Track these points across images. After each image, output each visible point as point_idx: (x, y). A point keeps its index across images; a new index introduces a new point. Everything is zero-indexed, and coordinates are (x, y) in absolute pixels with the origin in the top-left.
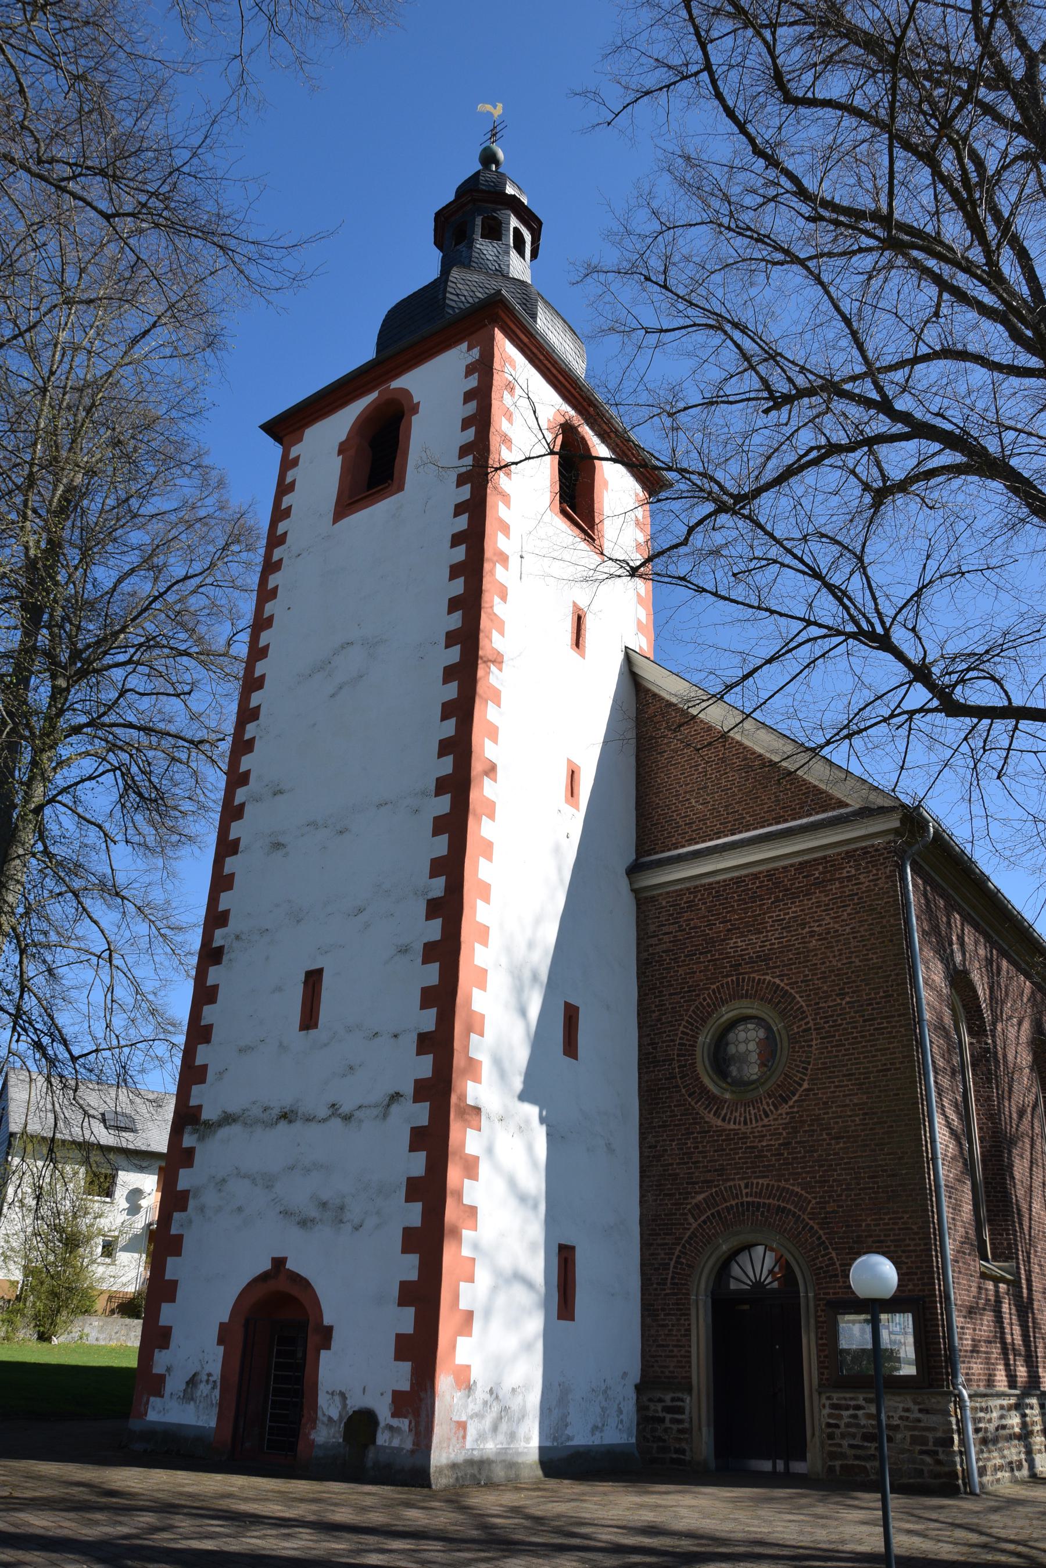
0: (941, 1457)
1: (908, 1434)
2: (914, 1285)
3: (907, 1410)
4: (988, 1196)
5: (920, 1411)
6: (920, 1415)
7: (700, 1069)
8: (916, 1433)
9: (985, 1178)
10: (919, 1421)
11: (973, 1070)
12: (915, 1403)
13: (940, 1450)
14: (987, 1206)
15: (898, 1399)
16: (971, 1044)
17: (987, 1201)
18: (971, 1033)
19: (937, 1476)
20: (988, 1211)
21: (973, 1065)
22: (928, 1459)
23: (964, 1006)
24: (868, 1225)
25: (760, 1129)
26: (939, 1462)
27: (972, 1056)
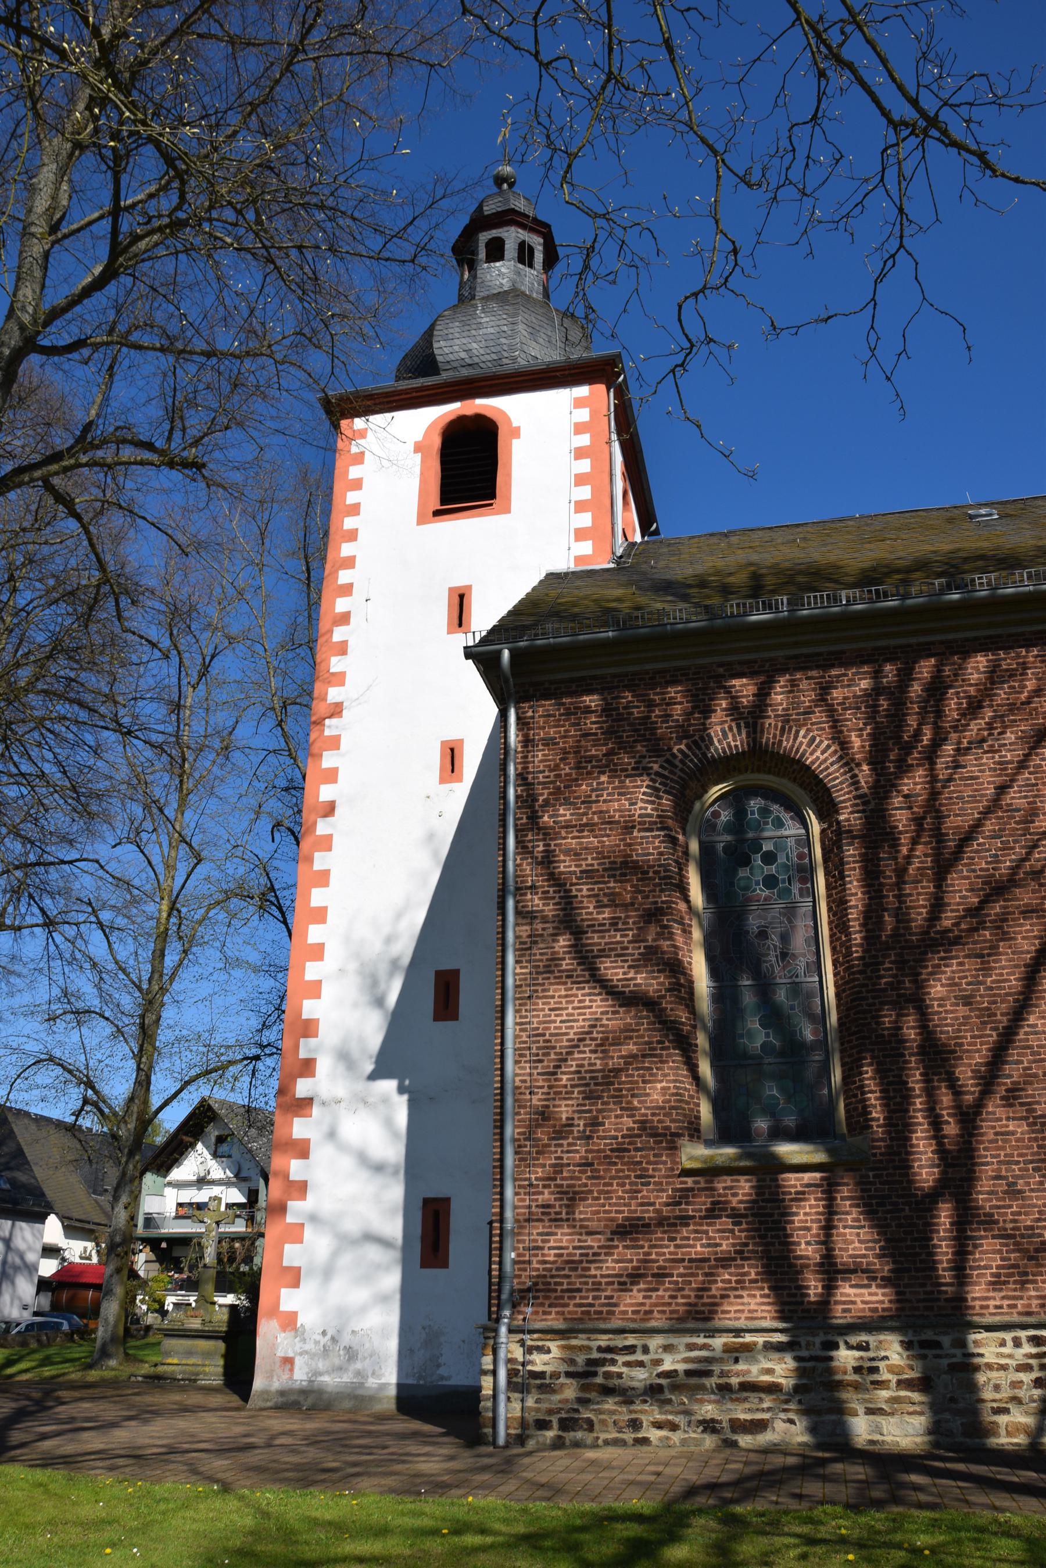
9: (839, 1019)
11: (826, 868)
14: (842, 1059)
18: (821, 818)
20: (843, 1065)
23: (801, 785)
25: (580, 992)
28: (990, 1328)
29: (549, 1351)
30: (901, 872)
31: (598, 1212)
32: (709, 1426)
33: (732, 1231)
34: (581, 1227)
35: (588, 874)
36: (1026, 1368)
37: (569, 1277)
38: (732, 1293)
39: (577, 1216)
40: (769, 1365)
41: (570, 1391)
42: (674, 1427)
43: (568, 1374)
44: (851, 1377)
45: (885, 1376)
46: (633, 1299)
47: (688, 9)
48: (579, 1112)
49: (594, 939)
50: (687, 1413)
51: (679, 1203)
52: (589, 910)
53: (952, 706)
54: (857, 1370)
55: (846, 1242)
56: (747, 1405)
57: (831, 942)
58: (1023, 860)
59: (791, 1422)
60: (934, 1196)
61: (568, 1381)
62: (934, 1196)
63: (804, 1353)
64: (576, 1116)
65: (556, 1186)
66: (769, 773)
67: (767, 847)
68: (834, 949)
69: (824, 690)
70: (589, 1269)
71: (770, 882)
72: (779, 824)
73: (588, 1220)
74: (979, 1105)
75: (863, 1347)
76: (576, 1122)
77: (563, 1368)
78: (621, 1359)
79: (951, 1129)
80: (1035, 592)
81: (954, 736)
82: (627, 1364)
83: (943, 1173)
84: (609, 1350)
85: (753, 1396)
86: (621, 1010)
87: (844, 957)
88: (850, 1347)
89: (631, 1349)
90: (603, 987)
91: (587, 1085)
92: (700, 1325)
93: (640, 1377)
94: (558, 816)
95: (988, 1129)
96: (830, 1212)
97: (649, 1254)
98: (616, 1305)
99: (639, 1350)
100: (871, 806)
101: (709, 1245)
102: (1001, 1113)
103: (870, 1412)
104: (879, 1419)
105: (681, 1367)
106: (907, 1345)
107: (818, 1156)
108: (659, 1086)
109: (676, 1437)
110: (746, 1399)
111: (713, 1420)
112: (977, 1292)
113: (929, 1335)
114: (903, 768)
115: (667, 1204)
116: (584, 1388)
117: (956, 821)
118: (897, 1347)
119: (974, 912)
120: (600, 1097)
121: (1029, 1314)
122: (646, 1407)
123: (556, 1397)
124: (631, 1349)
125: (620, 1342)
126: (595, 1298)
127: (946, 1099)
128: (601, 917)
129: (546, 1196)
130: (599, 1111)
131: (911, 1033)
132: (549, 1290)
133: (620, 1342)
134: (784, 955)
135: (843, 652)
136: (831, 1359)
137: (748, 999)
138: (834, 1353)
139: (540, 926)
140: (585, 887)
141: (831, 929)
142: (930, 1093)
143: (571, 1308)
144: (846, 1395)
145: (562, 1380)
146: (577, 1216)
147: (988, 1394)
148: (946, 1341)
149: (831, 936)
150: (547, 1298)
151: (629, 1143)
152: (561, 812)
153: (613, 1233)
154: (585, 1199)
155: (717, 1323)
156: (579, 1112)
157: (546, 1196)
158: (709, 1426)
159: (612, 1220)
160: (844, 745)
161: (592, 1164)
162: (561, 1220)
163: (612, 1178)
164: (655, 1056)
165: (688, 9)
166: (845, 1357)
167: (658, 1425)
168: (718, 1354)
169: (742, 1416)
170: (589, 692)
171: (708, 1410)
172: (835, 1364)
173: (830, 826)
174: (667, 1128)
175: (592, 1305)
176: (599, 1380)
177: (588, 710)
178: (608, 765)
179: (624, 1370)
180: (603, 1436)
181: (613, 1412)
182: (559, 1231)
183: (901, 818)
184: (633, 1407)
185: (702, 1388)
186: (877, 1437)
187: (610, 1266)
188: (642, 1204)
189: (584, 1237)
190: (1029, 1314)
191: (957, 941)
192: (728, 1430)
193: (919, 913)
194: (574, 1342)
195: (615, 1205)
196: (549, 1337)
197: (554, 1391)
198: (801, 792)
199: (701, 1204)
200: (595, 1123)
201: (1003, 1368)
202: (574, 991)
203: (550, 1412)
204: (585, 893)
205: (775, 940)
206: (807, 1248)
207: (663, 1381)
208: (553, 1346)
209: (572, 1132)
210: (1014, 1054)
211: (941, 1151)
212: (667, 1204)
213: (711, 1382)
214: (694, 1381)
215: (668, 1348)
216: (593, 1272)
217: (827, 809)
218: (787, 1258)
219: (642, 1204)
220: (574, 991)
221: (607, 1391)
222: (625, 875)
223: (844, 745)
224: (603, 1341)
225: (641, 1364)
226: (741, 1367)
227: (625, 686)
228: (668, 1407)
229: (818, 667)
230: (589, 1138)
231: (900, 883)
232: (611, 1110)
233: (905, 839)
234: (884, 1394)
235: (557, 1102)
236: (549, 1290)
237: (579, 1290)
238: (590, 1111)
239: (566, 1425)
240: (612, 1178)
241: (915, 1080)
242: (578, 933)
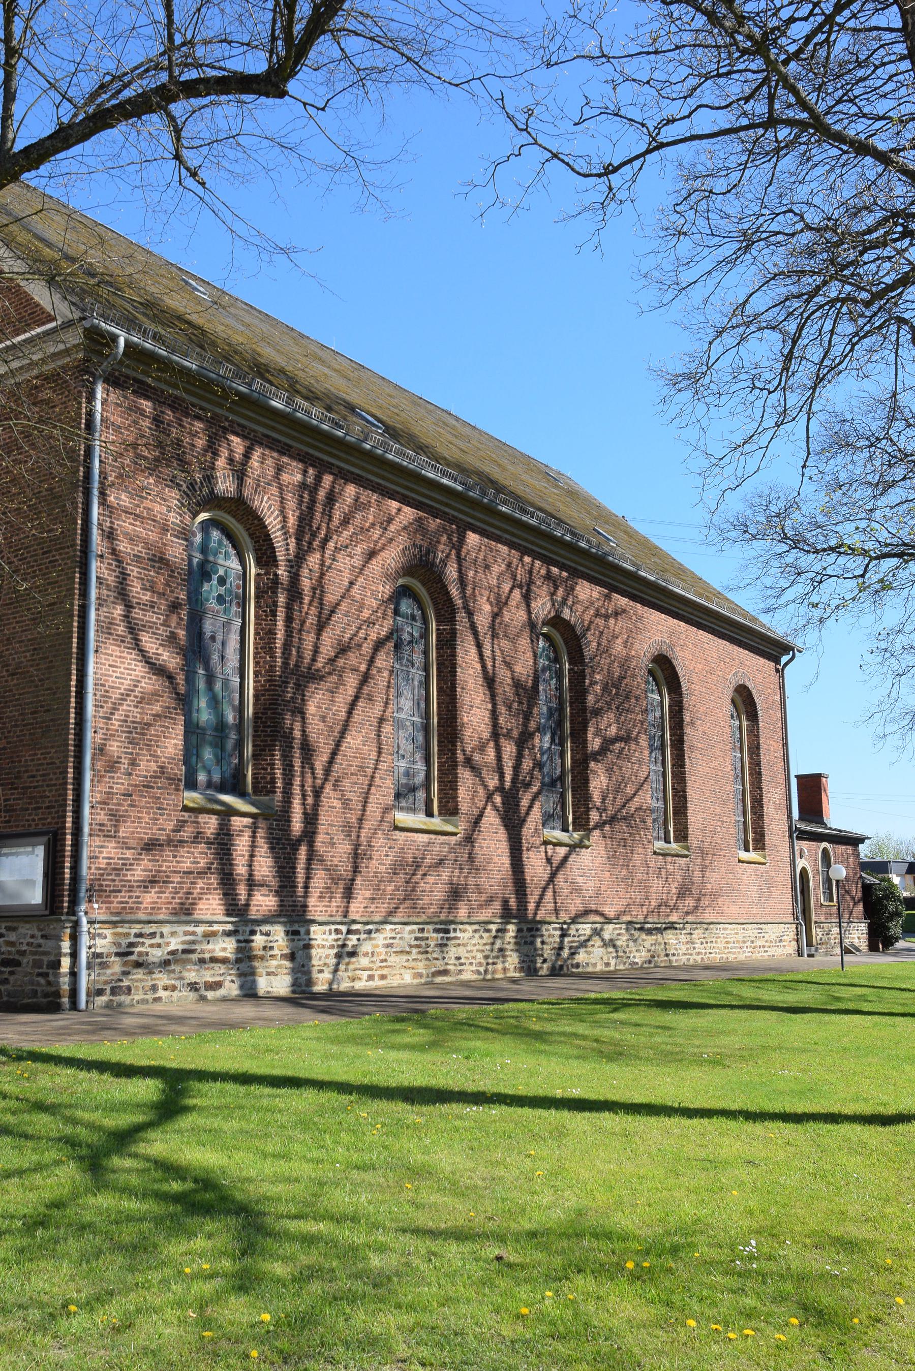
0: (51, 978)
1: (31, 958)
2: (53, 818)
3: (32, 936)
4: (255, 731)
5: (42, 936)
6: (41, 941)
7: (419, 585)
8: (37, 957)
9: (255, 713)
10: (40, 946)
11: (257, 603)
12: (40, 930)
13: (51, 971)
14: (254, 741)
15: (28, 926)
16: (258, 575)
17: (254, 736)
18: (259, 563)
19: (46, 995)
20: (254, 746)
21: (257, 597)
22: (42, 981)
23: (250, 535)
24: (26, 761)
25: (129, 656)
26: (49, 983)
27: (257, 588)
28: (321, 924)
29: (105, 937)
30: (303, 622)
31: (133, 833)
32: (193, 987)
33: (206, 854)
34: (124, 843)
35: (137, 558)
36: (332, 947)
37: (114, 880)
38: (204, 897)
39: (121, 834)
40: (224, 945)
41: (116, 967)
42: (174, 988)
43: (117, 954)
44: (261, 953)
45: (276, 952)
46: (149, 898)
47: (522, 130)
48: (126, 753)
49: (137, 613)
50: (181, 978)
51: (179, 831)
52: (136, 589)
53: (337, 515)
54: (265, 948)
55: (261, 866)
56: (212, 972)
57: (255, 658)
58: (355, 635)
59: (233, 981)
60: (299, 841)
61: (117, 959)
62: (299, 841)
63: (241, 938)
64: (123, 756)
65: (109, 810)
66: (234, 517)
67: (221, 572)
68: (257, 663)
69: (279, 469)
70: (126, 875)
71: (220, 599)
72: (227, 556)
73: (128, 838)
74: (322, 787)
75: (267, 934)
76: (123, 760)
77: (114, 950)
78: (148, 942)
79: (310, 800)
80: (317, 426)
81: (335, 537)
82: (151, 946)
83: (305, 827)
84: (140, 935)
85: (216, 966)
86: (154, 677)
87: (267, 671)
88: (262, 934)
89: (153, 935)
90: (144, 656)
91: (130, 732)
92: (184, 918)
93: (157, 955)
94: (120, 499)
95: (324, 801)
96: (253, 846)
97: (161, 866)
98: (141, 903)
99: (158, 935)
100: (294, 570)
101: (194, 863)
102: (332, 794)
103: (268, 974)
104: (272, 978)
105: (180, 947)
106: (287, 933)
107: (253, 810)
108: (173, 741)
109: (176, 994)
110: (213, 968)
111: (196, 983)
112: (312, 901)
113: (296, 927)
114: (310, 549)
115: (174, 831)
116: (125, 964)
117: (330, 598)
118: (282, 934)
119: (332, 661)
120: (138, 744)
121: (331, 916)
122: (161, 975)
123: (109, 971)
124: (153, 935)
125: (148, 929)
126: (130, 897)
127: (309, 781)
128: (145, 598)
129: (102, 817)
130: (137, 754)
131: (297, 734)
132: (102, 891)
133: (148, 929)
134: (223, 657)
135: (291, 447)
136: (252, 941)
137: (202, 685)
138: (253, 938)
139: (105, 592)
140: (136, 569)
141: (256, 648)
142: (303, 774)
143: (115, 905)
144: (256, 964)
145: (113, 959)
146: (121, 834)
147: (315, 962)
148: (302, 930)
149: (255, 653)
150: (100, 896)
151: (155, 783)
152: (123, 497)
153: (142, 849)
154: (125, 822)
155: (197, 916)
156: (126, 753)
157: (102, 817)
158: (193, 987)
159: (142, 839)
160: (285, 519)
161: (131, 795)
162: (110, 836)
163: (142, 807)
164: (172, 718)
165: (522, 130)
166: (259, 940)
167: (165, 988)
168: (199, 938)
169: (211, 980)
170: (147, 398)
171: (191, 975)
172: (254, 944)
173: (267, 573)
174: (176, 774)
175: (127, 903)
176: (133, 958)
177: (142, 412)
178: (154, 467)
179: (149, 950)
180: (137, 998)
181: (141, 980)
182: (110, 845)
183: (306, 584)
184: (154, 976)
185: (189, 961)
186: (270, 989)
187: (138, 873)
188: (160, 829)
189: (125, 851)
190: (331, 916)
191: (322, 678)
192: (203, 989)
193: (308, 655)
194: (119, 930)
195: (145, 828)
196: (106, 926)
197: (108, 967)
198: (248, 539)
199: (187, 833)
200: (133, 763)
201: (324, 947)
202: (125, 655)
203: (106, 983)
204: (135, 574)
205: (218, 645)
206: (241, 869)
207: (170, 957)
208: (108, 932)
209: (120, 768)
210: (339, 758)
211: (305, 814)
212: (174, 831)
213: (194, 957)
214: (184, 956)
215: (173, 934)
216: (129, 878)
217: (266, 557)
218: (232, 874)
219: (160, 829)
220: (125, 655)
221: (138, 965)
222: (160, 568)
223: (285, 519)
224: (136, 929)
225: (159, 946)
226: (210, 947)
227: (169, 405)
228: (172, 975)
229: (278, 451)
230: (130, 774)
231: (300, 630)
232: (144, 755)
233: (307, 600)
234: (274, 963)
235: (112, 743)
236: (102, 891)
237: (120, 891)
238: (131, 754)
239: (114, 991)
240: (142, 807)
241: (297, 764)
242: (129, 606)
